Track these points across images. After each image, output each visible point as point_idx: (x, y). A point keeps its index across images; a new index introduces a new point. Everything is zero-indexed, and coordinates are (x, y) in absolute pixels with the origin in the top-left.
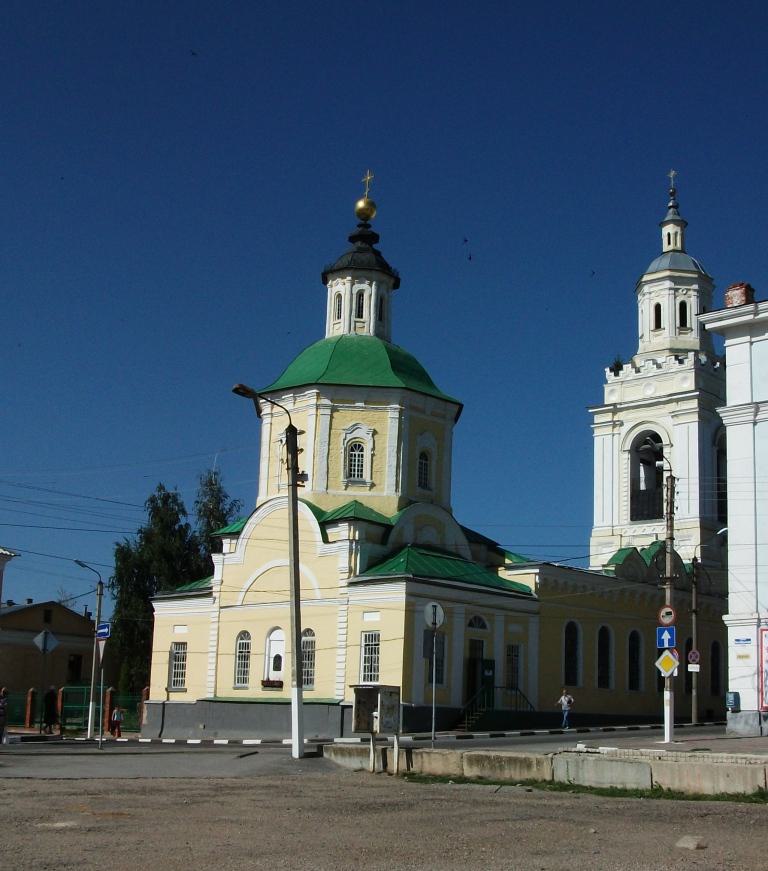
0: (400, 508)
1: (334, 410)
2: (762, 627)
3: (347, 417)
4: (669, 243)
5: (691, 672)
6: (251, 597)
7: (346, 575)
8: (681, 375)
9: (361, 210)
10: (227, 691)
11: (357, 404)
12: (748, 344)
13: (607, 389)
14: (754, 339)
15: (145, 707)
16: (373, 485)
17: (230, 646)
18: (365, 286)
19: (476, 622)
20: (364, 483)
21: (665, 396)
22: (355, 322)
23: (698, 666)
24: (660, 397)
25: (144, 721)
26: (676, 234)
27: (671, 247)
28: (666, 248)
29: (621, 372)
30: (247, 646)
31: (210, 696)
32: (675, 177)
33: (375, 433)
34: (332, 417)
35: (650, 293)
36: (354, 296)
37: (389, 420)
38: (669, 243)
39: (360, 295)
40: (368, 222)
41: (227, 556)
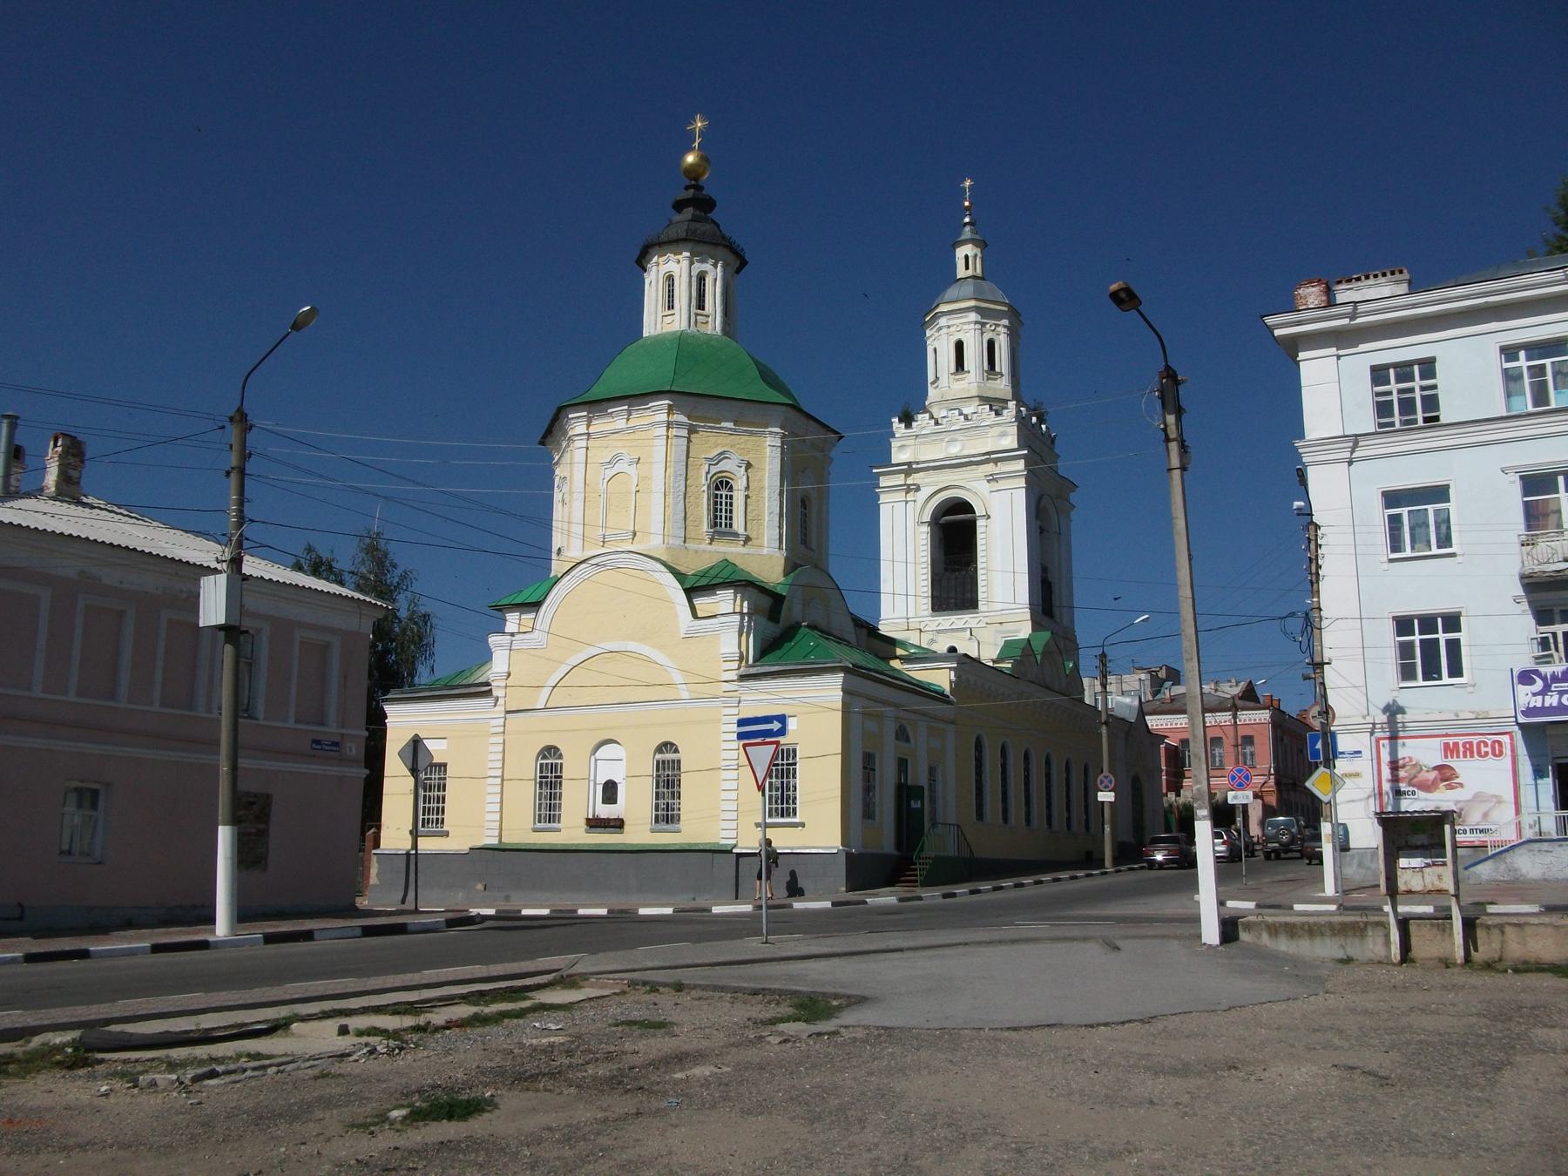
0: (786, 574)
1: (692, 430)
2: (1378, 735)
3: (711, 442)
4: (967, 268)
5: (1103, 802)
6: (559, 698)
7: (735, 665)
8: (997, 430)
9: (692, 165)
10: (522, 830)
11: (724, 424)
12: (1335, 358)
13: (895, 444)
14: (1341, 352)
15: (374, 859)
16: (748, 539)
17: (526, 767)
18: (707, 267)
19: (902, 734)
20: (736, 535)
21: (979, 455)
22: (697, 315)
23: (1113, 794)
24: (973, 456)
25: (373, 880)
26: (976, 255)
27: (970, 272)
28: (961, 272)
29: (914, 424)
30: (676, 764)
31: (494, 841)
32: (970, 186)
33: (749, 466)
34: (689, 441)
35: (949, 327)
36: (694, 279)
37: (768, 449)
38: (967, 268)
39: (701, 278)
40: (700, 183)
41: (517, 637)
